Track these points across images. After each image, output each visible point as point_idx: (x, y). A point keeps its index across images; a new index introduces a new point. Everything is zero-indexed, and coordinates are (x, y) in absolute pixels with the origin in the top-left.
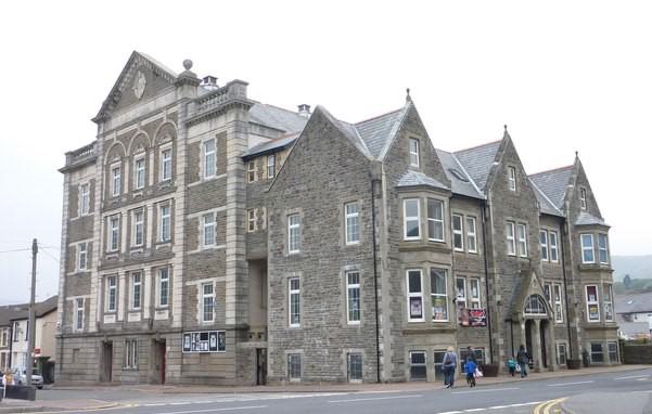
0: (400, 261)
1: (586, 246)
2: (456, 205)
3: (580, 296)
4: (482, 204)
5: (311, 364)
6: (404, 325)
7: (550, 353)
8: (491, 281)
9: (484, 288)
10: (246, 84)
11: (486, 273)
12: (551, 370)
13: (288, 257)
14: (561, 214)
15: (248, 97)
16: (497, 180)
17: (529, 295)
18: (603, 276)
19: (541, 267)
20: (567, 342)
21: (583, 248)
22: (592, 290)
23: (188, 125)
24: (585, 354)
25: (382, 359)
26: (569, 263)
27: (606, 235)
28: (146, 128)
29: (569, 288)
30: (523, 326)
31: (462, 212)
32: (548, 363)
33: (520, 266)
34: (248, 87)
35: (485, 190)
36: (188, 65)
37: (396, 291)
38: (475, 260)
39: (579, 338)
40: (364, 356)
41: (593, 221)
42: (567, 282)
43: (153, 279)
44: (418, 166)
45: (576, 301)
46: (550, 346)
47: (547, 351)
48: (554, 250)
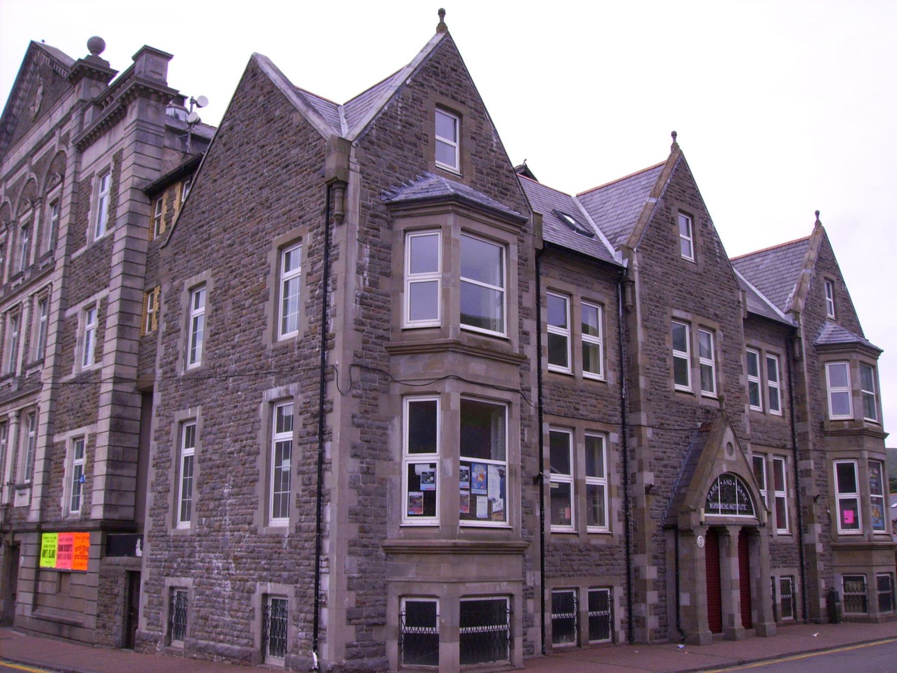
0: (387, 376)
1: (837, 385)
2: (554, 272)
3: (825, 484)
4: (614, 276)
5: (203, 612)
6: (393, 537)
7: (760, 597)
8: (633, 442)
9: (617, 457)
10: (169, 57)
11: (624, 425)
12: (761, 633)
13: (184, 379)
14: (789, 319)
15: (169, 86)
16: (656, 235)
17: (716, 473)
18: (869, 443)
19: (746, 421)
20: (796, 572)
21: (831, 390)
22: (846, 475)
23: (82, 146)
24: (831, 596)
25: (325, 613)
26: (802, 417)
27: (875, 367)
28: (36, 169)
29: (802, 465)
30: (701, 541)
31: (571, 288)
32: (755, 619)
33: (699, 413)
34: (171, 64)
35: (626, 251)
36: (97, 45)
37: (371, 447)
38: (598, 395)
39: (820, 566)
40: (292, 605)
41: (849, 337)
42: (799, 454)
43: (18, 431)
44: (456, 169)
45: (814, 491)
46: (759, 582)
47: (754, 594)
48: (773, 391)
